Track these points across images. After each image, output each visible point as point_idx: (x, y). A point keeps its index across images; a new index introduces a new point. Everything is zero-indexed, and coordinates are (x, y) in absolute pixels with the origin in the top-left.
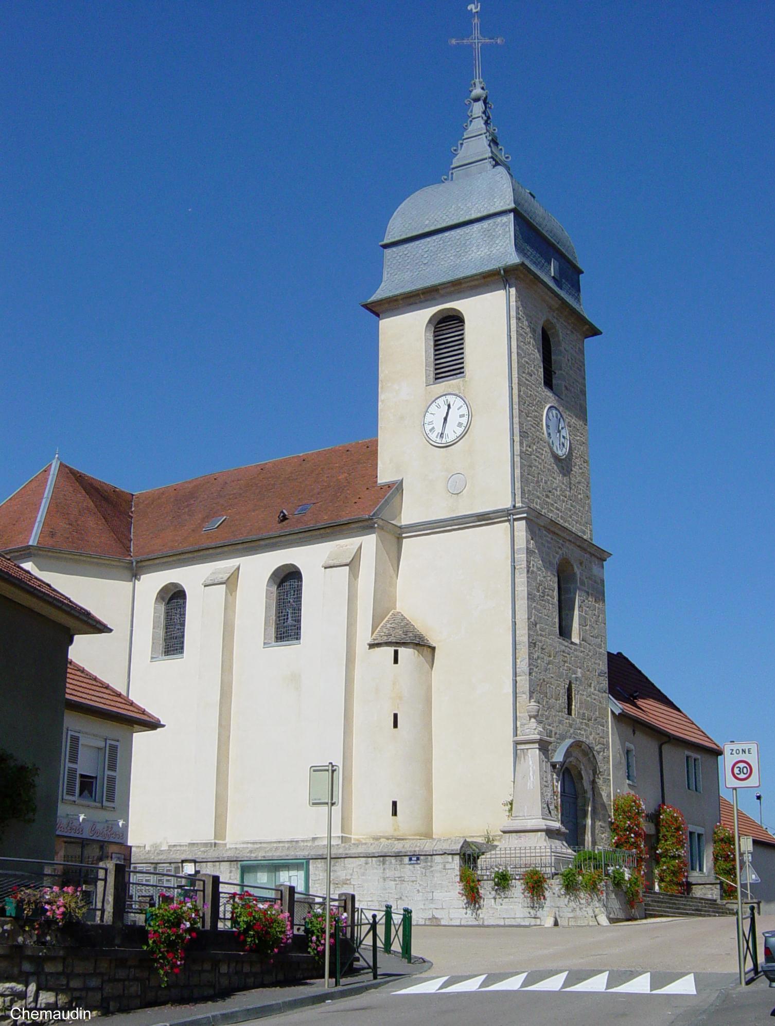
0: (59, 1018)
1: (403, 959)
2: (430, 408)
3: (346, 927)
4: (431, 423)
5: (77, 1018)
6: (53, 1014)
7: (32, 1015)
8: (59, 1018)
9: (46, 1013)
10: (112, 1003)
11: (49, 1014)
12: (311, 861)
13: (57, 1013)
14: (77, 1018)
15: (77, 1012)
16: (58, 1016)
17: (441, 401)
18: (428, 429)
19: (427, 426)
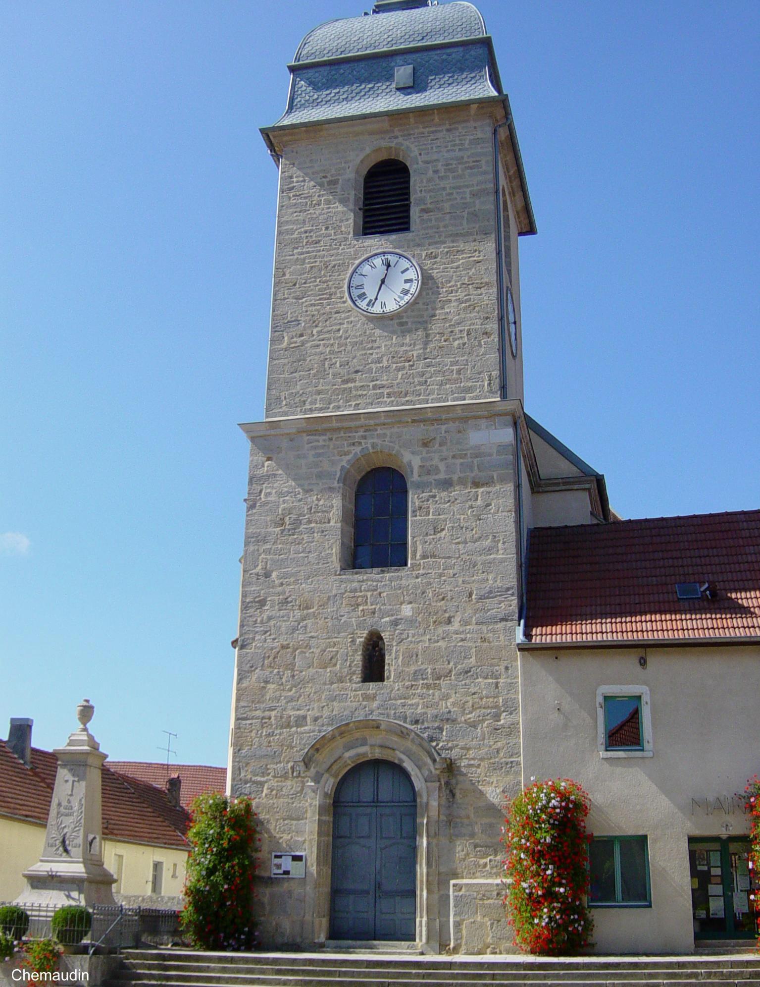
0: (59, 979)
1: (189, 809)
2: (352, 282)
3: (708, 864)
4: (360, 287)
5: (76, 979)
6: (52, 976)
7: (32, 976)
8: (59, 979)
9: (46, 974)
10: (699, 868)
11: (48, 975)
12: (711, 853)
13: (57, 974)
14: (76, 979)
15: (76, 974)
16: (57, 978)
17: (378, 261)
18: (365, 306)
19: (354, 290)
